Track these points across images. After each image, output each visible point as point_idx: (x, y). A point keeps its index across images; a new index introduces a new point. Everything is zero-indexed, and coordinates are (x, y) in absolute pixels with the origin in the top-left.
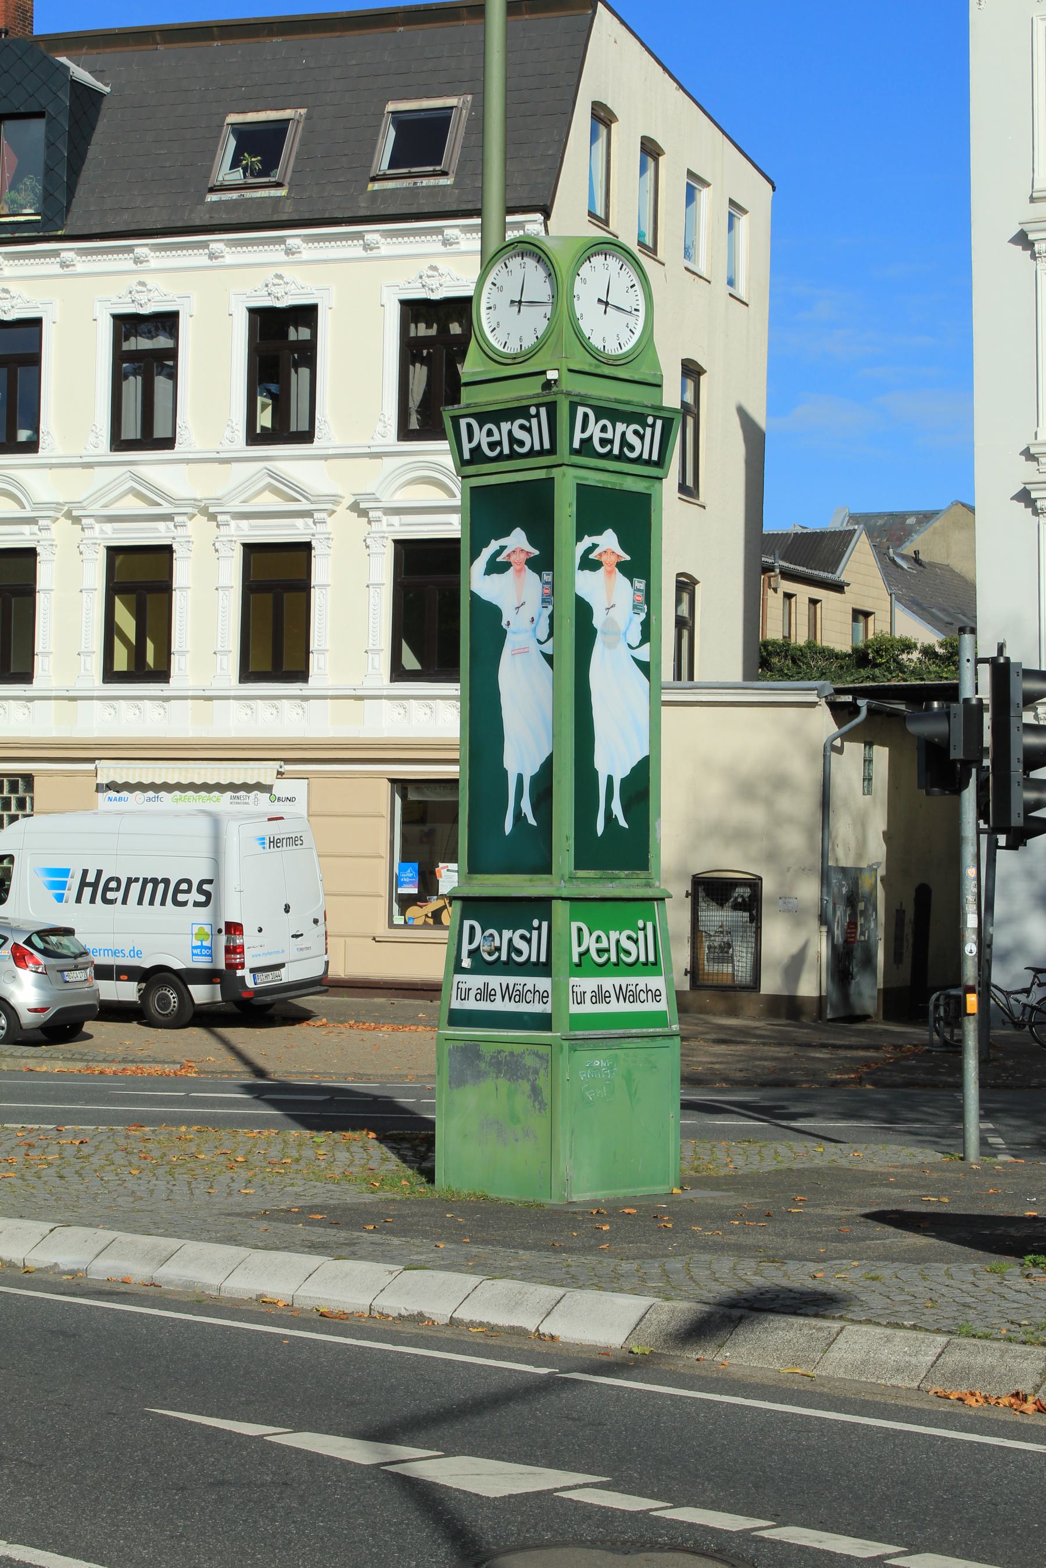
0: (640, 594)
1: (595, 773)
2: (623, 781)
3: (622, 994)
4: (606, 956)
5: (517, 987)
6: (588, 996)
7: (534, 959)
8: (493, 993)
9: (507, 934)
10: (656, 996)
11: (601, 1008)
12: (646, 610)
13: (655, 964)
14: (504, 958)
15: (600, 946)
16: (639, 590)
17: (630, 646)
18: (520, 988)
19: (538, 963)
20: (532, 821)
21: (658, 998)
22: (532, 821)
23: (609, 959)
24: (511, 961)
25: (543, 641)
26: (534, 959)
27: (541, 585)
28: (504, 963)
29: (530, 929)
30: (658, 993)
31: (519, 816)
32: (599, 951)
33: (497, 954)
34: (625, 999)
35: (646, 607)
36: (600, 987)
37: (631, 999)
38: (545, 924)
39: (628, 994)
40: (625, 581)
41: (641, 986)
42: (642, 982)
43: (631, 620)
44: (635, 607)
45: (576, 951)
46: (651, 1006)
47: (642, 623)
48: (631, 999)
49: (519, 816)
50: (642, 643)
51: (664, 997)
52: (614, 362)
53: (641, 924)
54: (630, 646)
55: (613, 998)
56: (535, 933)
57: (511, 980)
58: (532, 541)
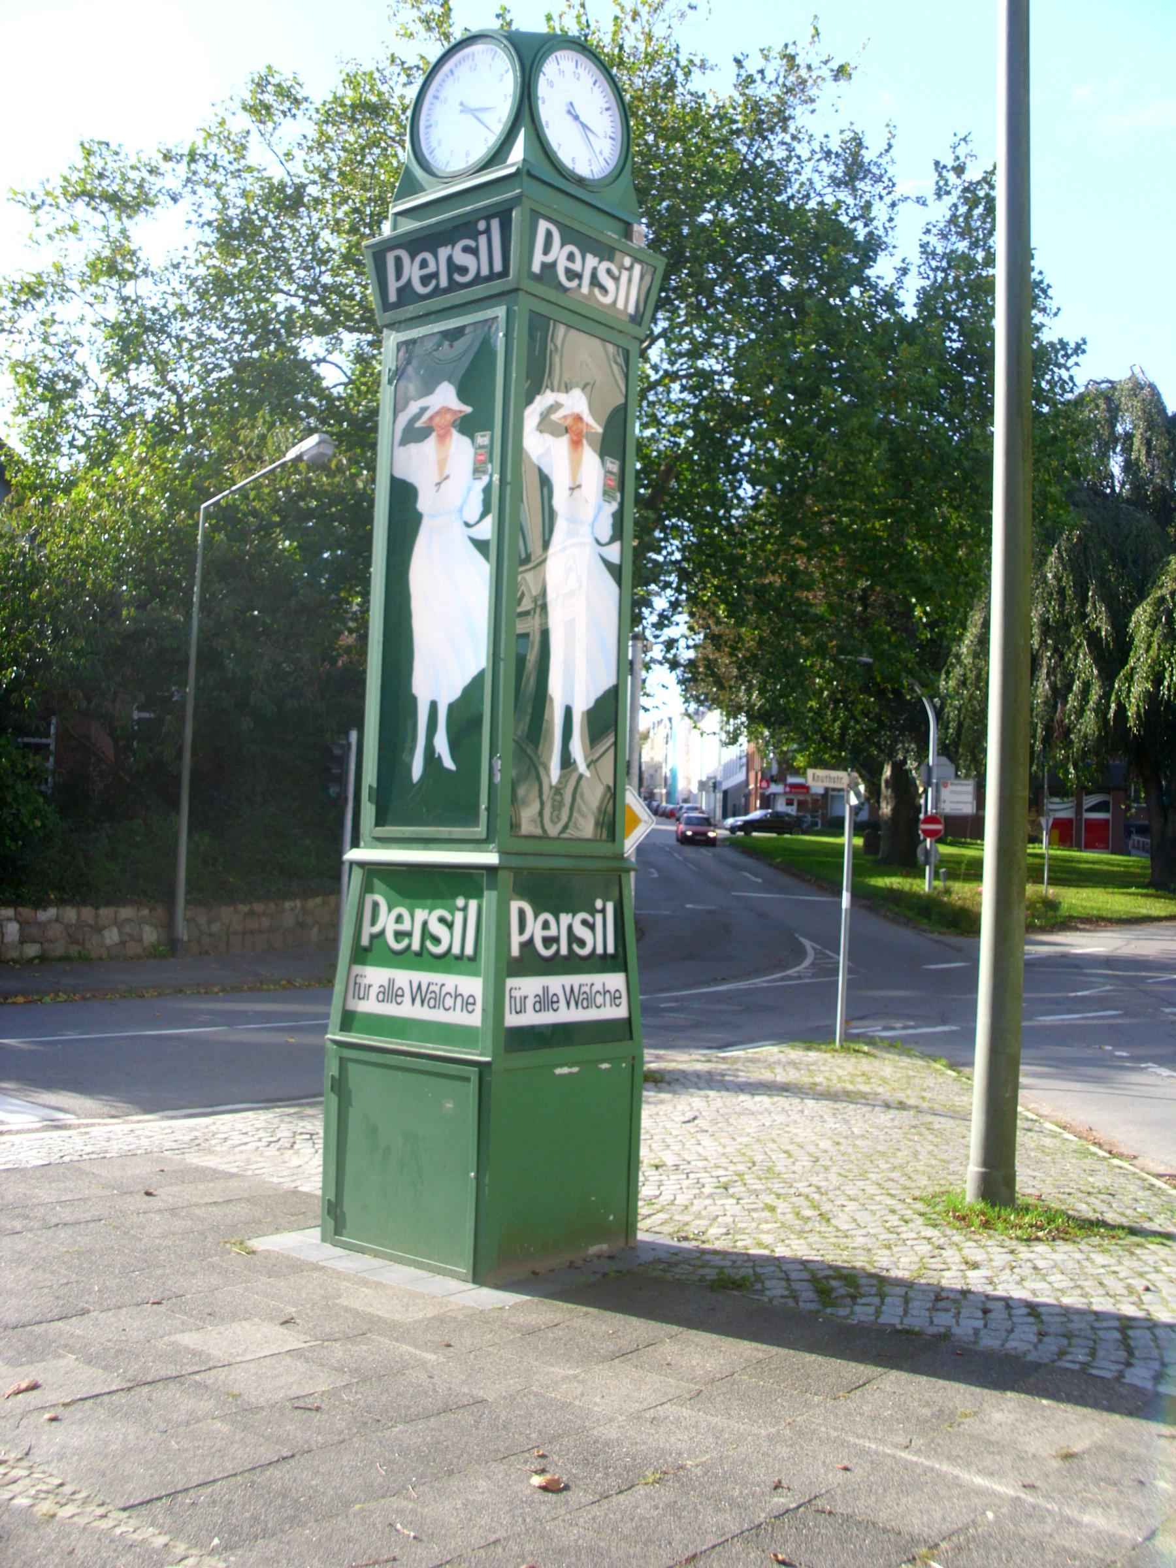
0: (612, 477)
1: (413, 700)
2: (451, 707)
3: (420, 995)
4: (405, 942)
5: (432, 988)
6: (530, 1003)
7: (600, 950)
8: (400, 992)
9: (565, 919)
10: (468, 1004)
11: (547, 1018)
12: (619, 499)
13: (473, 959)
14: (416, 946)
15: (400, 927)
16: (610, 472)
17: (598, 542)
18: (437, 989)
19: (605, 955)
20: (449, 763)
21: (470, 1008)
22: (449, 763)
23: (409, 946)
24: (425, 951)
25: (472, 522)
26: (600, 950)
27: (602, 472)
28: (565, 958)
29: (593, 911)
30: (471, 1000)
31: (431, 757)
32: (547, 942)
33: (405, 942)
34: (423, 1002)
35: (618, 495)
36: (391, 982)
37: (432, 1003)
38: (610, 907)
39: (429, 996)
40: (466, 441)
41: (598, 987)
42: (451, 981)
43: (469, 490)
44: (605, 493)
45: (516, 940)
46: (458, 1017)
47: (614, 515)
48: (432, 1003)
49: (431, 757)
50: (612, 540)
51: (479, 1007)
52: (580, 181)
53: (599, 904)
54: (598, 542)
55: (562, 1003)
56: (599, 917)
57: (424, 977)
58: (463, 396)
